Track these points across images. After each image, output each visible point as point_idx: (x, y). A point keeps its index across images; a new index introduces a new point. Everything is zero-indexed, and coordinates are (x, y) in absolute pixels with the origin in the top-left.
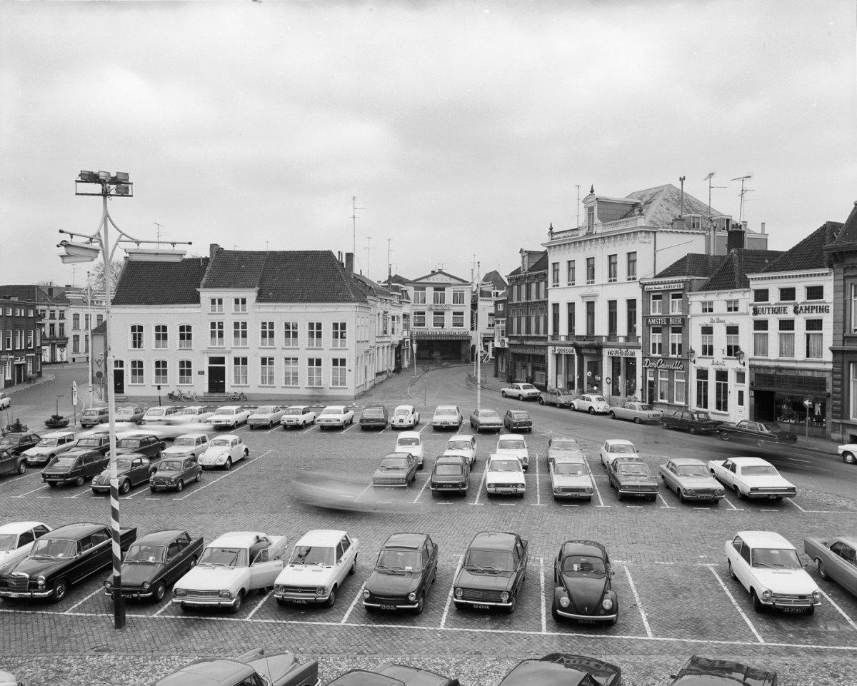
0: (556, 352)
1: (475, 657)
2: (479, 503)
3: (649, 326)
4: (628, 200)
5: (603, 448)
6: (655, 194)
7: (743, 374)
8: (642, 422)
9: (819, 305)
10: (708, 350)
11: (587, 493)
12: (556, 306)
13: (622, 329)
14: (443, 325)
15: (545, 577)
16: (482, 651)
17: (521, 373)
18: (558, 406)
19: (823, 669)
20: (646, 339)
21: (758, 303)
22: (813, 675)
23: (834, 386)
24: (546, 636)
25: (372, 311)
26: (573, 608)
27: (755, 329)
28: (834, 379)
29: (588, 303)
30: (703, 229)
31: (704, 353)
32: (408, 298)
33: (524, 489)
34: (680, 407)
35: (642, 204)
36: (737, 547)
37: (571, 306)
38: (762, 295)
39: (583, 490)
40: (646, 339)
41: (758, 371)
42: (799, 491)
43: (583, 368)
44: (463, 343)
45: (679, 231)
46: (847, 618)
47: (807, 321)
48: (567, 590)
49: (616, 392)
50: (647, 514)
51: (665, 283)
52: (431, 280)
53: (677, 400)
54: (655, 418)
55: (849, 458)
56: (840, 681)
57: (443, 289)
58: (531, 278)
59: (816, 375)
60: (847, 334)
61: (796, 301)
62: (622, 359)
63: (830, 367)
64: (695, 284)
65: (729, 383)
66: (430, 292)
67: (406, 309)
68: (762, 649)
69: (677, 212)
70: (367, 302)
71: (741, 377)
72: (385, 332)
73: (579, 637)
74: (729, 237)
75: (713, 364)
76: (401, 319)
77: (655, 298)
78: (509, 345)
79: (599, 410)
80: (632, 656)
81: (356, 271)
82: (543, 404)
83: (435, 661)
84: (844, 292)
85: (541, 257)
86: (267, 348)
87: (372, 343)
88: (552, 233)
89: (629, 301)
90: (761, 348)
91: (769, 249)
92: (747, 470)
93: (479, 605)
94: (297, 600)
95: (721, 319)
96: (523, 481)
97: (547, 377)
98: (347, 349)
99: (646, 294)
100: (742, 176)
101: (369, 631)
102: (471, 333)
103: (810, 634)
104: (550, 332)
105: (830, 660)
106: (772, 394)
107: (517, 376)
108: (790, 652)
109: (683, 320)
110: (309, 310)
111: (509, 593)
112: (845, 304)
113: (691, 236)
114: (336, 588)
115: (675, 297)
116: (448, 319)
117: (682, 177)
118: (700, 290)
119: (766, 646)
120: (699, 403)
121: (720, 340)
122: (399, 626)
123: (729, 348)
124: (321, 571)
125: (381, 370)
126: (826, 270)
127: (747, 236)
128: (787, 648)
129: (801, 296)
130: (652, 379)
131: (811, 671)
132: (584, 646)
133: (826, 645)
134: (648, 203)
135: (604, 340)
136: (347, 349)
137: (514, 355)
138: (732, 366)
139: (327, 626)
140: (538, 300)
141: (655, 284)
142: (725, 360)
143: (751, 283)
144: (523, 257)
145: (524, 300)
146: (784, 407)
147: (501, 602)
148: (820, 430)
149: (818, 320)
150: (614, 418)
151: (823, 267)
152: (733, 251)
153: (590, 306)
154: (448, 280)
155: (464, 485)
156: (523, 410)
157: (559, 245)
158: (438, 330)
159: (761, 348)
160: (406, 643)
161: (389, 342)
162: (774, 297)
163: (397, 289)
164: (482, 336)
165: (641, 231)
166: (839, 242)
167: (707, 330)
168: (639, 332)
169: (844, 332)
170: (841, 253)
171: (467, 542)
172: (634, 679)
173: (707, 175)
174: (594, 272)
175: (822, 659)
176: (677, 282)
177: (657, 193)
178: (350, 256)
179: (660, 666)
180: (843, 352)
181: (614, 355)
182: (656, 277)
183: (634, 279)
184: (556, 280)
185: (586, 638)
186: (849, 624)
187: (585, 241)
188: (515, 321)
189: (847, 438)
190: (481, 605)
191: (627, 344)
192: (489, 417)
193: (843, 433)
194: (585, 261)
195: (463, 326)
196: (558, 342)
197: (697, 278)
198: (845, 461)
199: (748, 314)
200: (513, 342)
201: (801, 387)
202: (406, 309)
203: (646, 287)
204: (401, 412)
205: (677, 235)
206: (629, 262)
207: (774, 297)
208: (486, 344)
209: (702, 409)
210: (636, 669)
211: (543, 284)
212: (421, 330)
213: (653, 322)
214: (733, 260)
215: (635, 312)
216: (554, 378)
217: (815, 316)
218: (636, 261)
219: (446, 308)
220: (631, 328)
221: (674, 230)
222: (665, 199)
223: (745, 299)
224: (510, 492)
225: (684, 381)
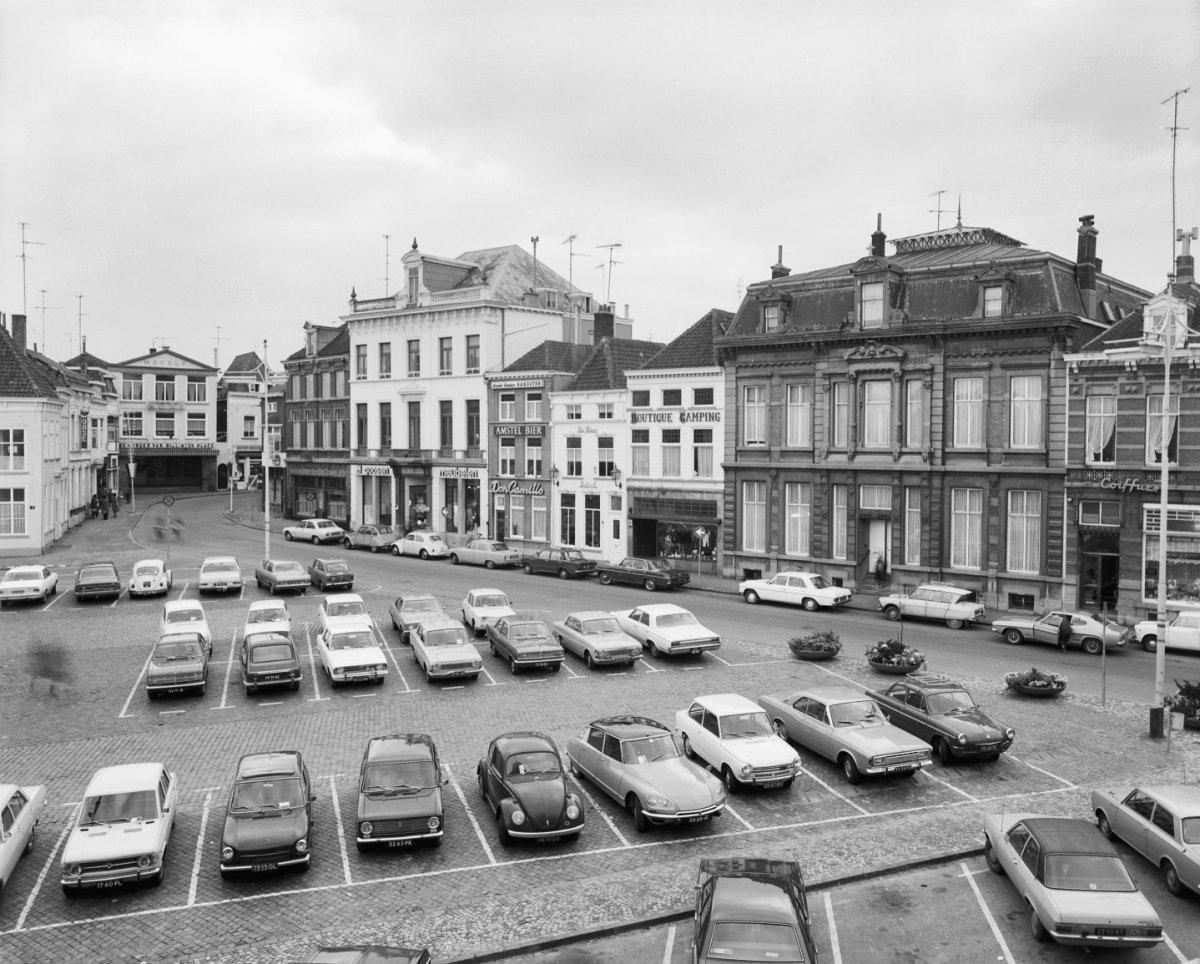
0: (364, 473)
1: (416, 915)
2: (226, 705)
3: (498, 436)
4: (460, 262)
5: (466, 601)
6: (498, 256)
7: (620, 499)
8: (497, 567)
9: (708, 411)
10: (576, 469)
11: (474, 668)
12: (362, 407)
13: (459, 440)
14: (171, 434)
15: (462, 789)
16: (421, 905)
17: (305, 505)
18: (374, 550)
19: (826, 848)
20: (493, 455)
21: (637, 407)
22: (818, 857)
23: (726, 510)
24: (498, 868)
25: (64, 412)
26: (530, 823)
27: (633, 441)
28: (726, 503)
29: (410, 403)
30: (560, 309)
31: (571, 472)
32: (114, 391)
33: (386, 672)
34: (540, 544)
35: (481, 269)
36: (697, 718)
37: (385, 407)
38: (642, 398)
39: (469, 665)
40: (493, 455)
41: (637, 494)
42: (725, 644)
43: (404, 494)
44: (204, 461)
45: (533, 309)
46: (825, 785)
47: (695, 431)
48: (519, 801)
49: (451, 527)
50: (556, 689)
51: (519, 379)
52: (151, 363)
53: (535, 535)
54: (514, 560)
55: (752, 597)
56: (846, 859)
57: (172, 378)
58: (322, 366)
59: (706, 497)
60: (740, 447)
61: (682, 406)
62: (460, 482)
63: (721, 487)
64: (558, 382)
65: (601, 510)
66: (149, 382)
67: (112, 408)
68: (755, 837)
69: (528, 284)
70: (56, 397)
71: (616, 502)
72: (84, 445)
73: (541, 861)
74: (596, 321)
75: (581, 486)
76: (105, 423)
77: (505, 398)
78: (288, 463)
79: (435, 554)
80: (615, 874)
81: (30, 346)
82: (351, 548)
83: (361, 932)
84: (737, 396)
85: (338, 334)
86: (11, 474)
87: (64, 463)
88: (355, 303)
89: (442, 403)
90: (640, 466)
91: (635, 337)
92: (665, 620)
93: (397, 841)
94: (104, 882)
95: (591, 429)
96: (384, 660)
97: (348, 509)
98: (27, 473)
99: (493, 392)
100: (612, 243)
101: (239, 908)
102: (219, 446)
103: (795, 810)
104: (354, 443)
105: (828, 836)
106: (654, 522)
107: (301, 509)
108: (785, 834)
109: (543, 429)
110: (12, 408)
111: (439, 817)
112: (737, 411)
113: (545, 317)
114: (169, 851)
115: (532, 397)
116: (181, 424)
117: (535, 238)
118: (564, 390)
119: (759, 833)
120: (564, 537)
121: (590, 456)
122: (284, 893)
123: (602, 465)
124: (140, 829)
125: (77, 506)
126: (717, 369)
127: (616, 321)
128: (780, 830)
129: (688, 399)
130: (502, 508)
131: (814, 853)
132: (552, 873)
133: (816, 819)
134: (489, 268)
135: (434, 455)
136: (27, 473)
137: (296, 477)
138: (605, 488)
139: (166, 913)
140: (333, 398)
141: (505, 379)
142: (597, 482)
143: (629, 382)
144: (310, 334)
145: (311, 397)
146: (668, 539)
147: (429, 832)
148: (710, 565)
149: (675, 431)
150: (457, 563)
151: (712, 365)
152: (604, 340)
153: (414, 408)
154: (181, 364)
155: (297, 673)
156: (339, 558)
157: (366, 320)
158: (164, 441)
159: (640, 466)
160: (305, 915)
161: (89, 460)
162: (656, 401)
163: (96, 376)
164: (236, 450)
165: (486, 307)
166: (732, 337)
167: (574, 443)
168: (484, 444)
169: (737, 445)
170: (734, 349)
171: (331, 757)
172: (630, 901)
173: (567, 237)
174: (418, 361)
175: (820, 836)
176: (534, 377)
177: (499, 256)
178: (19, 321)
179: (653, 879)
180: (736, 469)
181: (448, 477)
182: (505, 371)
183: (476, 372)
184: (362, 370)
185: (549, 861)
186: (828, 792)
187: (405, 316)
188: (297, 428)
189: (741, 573)
190: (400, 841)
191: (468, 461)
192: (291, 572)
193: (736, 567)
194: (406, 346)
195: (204, 434)
196: (366, 459)
197: (560, 373)
198: (747, 601)
199: (625, 421)
200: (294, 459)
201: (689, 513)
202: (112, 408)
203: (493, 384)
204: (143, 571)
205: (521, 313)
206: (469, 348)
207: (656, 401)
208: (241, 461)
209: (568, 546)
210: (628, 889)
211: (341, 376)
212: (199, 442)
213: (503, 431)
214: (600, 355)
215: (478, 419)
216: (360, 511)
217: (703, 425)
218: (478, 347)
219: (177, 407)
220: (472, 440)
221: (526, 308)
222: (511, 266)
223: (620, 402)
224: (367, 677)
225: (545, 509)
